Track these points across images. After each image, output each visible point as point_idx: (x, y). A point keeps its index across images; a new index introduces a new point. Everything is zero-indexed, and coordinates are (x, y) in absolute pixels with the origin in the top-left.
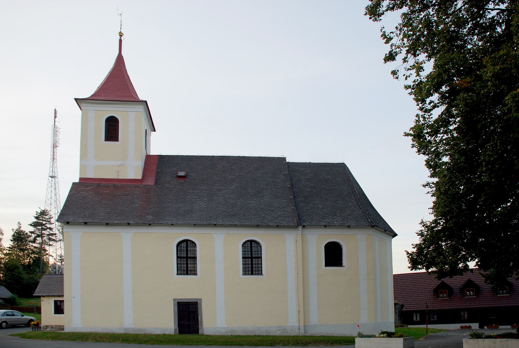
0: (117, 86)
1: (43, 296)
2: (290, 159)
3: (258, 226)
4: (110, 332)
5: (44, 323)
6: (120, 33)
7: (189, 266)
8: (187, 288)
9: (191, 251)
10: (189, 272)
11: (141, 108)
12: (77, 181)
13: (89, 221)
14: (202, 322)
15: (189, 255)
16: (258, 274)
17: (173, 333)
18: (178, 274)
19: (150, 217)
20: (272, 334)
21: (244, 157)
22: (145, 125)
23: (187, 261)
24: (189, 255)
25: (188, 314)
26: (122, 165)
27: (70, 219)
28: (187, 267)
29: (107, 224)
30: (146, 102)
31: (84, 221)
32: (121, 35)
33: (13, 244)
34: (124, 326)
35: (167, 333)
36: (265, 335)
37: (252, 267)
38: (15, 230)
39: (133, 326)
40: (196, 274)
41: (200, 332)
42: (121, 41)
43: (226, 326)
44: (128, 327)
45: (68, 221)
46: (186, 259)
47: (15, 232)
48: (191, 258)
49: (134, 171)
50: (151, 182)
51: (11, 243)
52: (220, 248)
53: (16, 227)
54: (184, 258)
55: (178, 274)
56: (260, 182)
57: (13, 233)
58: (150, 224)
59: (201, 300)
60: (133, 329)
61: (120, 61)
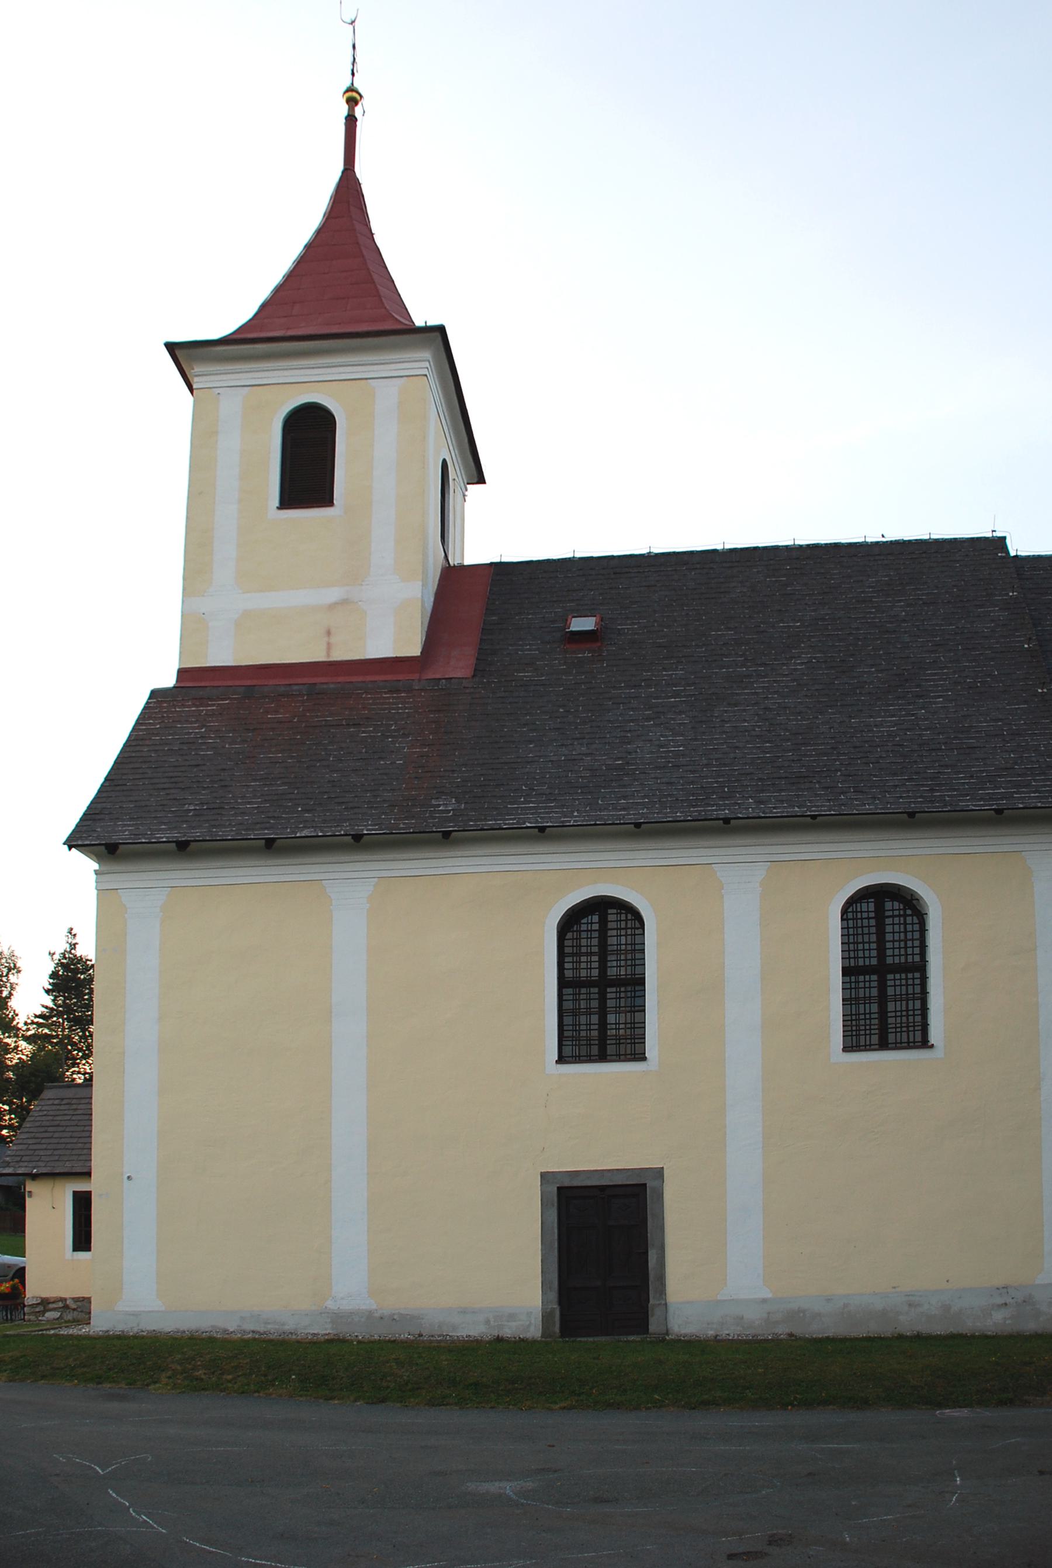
0: (339, 289)
1: (34, 1177)
2: (1018, 547)
3: (911, 815)
4: (272, 1329)
5: (35, 1289)
6: (351, 89)
7: (611, 1018)
8: (600, 1119)
9: (618, 952)
10: (611, 1050)
11: (420, 362)
12: (169, 680)
13: (197, 834)
14: (662, 1278)
15: (612, 972)
16: (910, 1045)
17: (535, 1331)
18: (561, 1060)
19: (447, 805)
20: (970, 1325)
21: (836, 546)
22: (440, 446)
23: (603, 999)
24: (612, 972)
25: (603, 1231)
26: (344, 602)
27: (122, 833)
28: (603, 1025)
29: (270, 843)
30: (441, 330)
31: (176, 835)
32: (353, 98)
33: (51, 1005)
34: (330, 1304)
35: (508, 1331)
36: (939, 1329)
37: (883, 1014)
38: (57, 957)
39: (364, 1303)
40: (644, 1059)
41: (654, 1326)
42: (351, 122)
43: (767, 1294)
44: (346, 1306)
45: (115, 839)
46: (601, 991)
47: (60, 964)
48: (618, 982)
49: (389, 626)
50: (458, 666)
51: (48, 1001)
52: (742, 927)
53: (61, 946)
54: (589, 983)
55: (561, 1060)
56: (906, 638)
57: (51, 967)
58: (446, 835)
59: (659, 1173)
60: (370, 1314)
61: (348, 198)
